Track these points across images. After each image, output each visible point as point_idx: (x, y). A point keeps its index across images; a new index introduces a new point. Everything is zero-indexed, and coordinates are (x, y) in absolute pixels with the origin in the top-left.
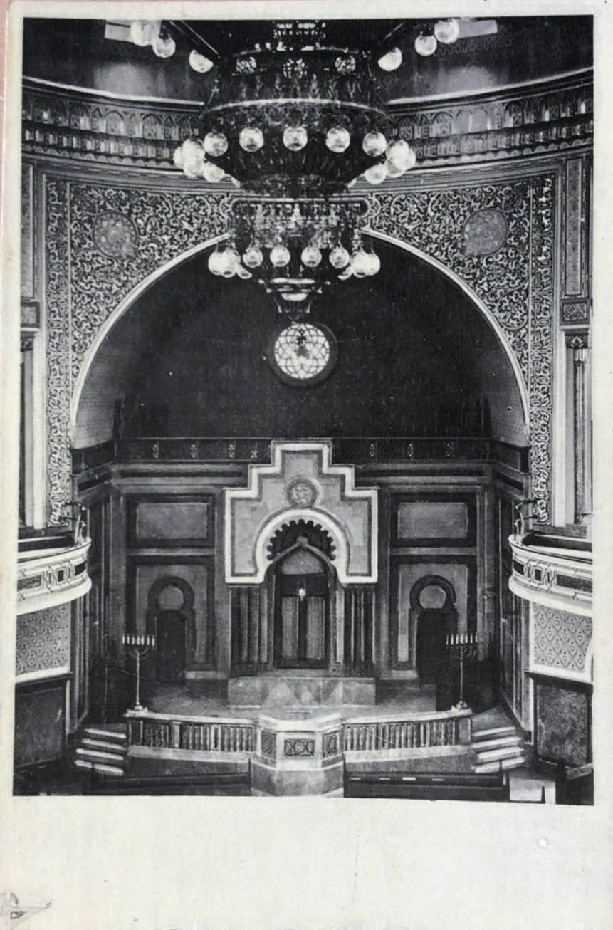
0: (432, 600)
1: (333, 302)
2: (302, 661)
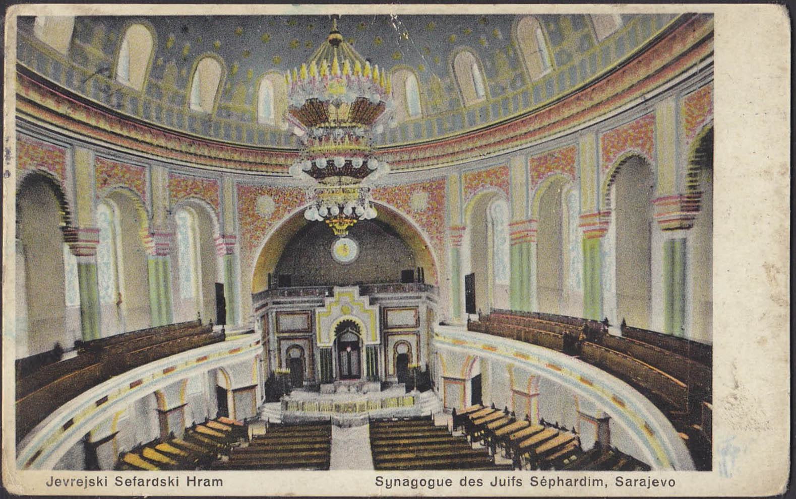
0: (402, 350)
1: (360, 230)
2: (350, 376)
